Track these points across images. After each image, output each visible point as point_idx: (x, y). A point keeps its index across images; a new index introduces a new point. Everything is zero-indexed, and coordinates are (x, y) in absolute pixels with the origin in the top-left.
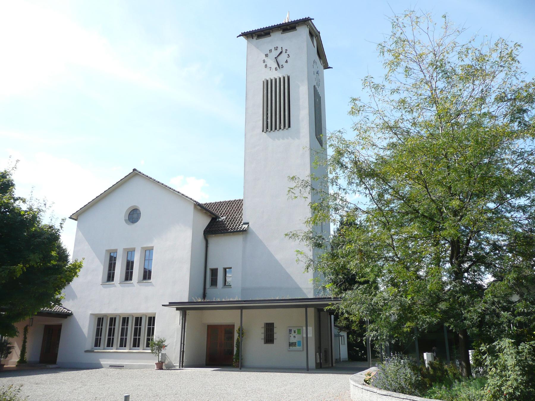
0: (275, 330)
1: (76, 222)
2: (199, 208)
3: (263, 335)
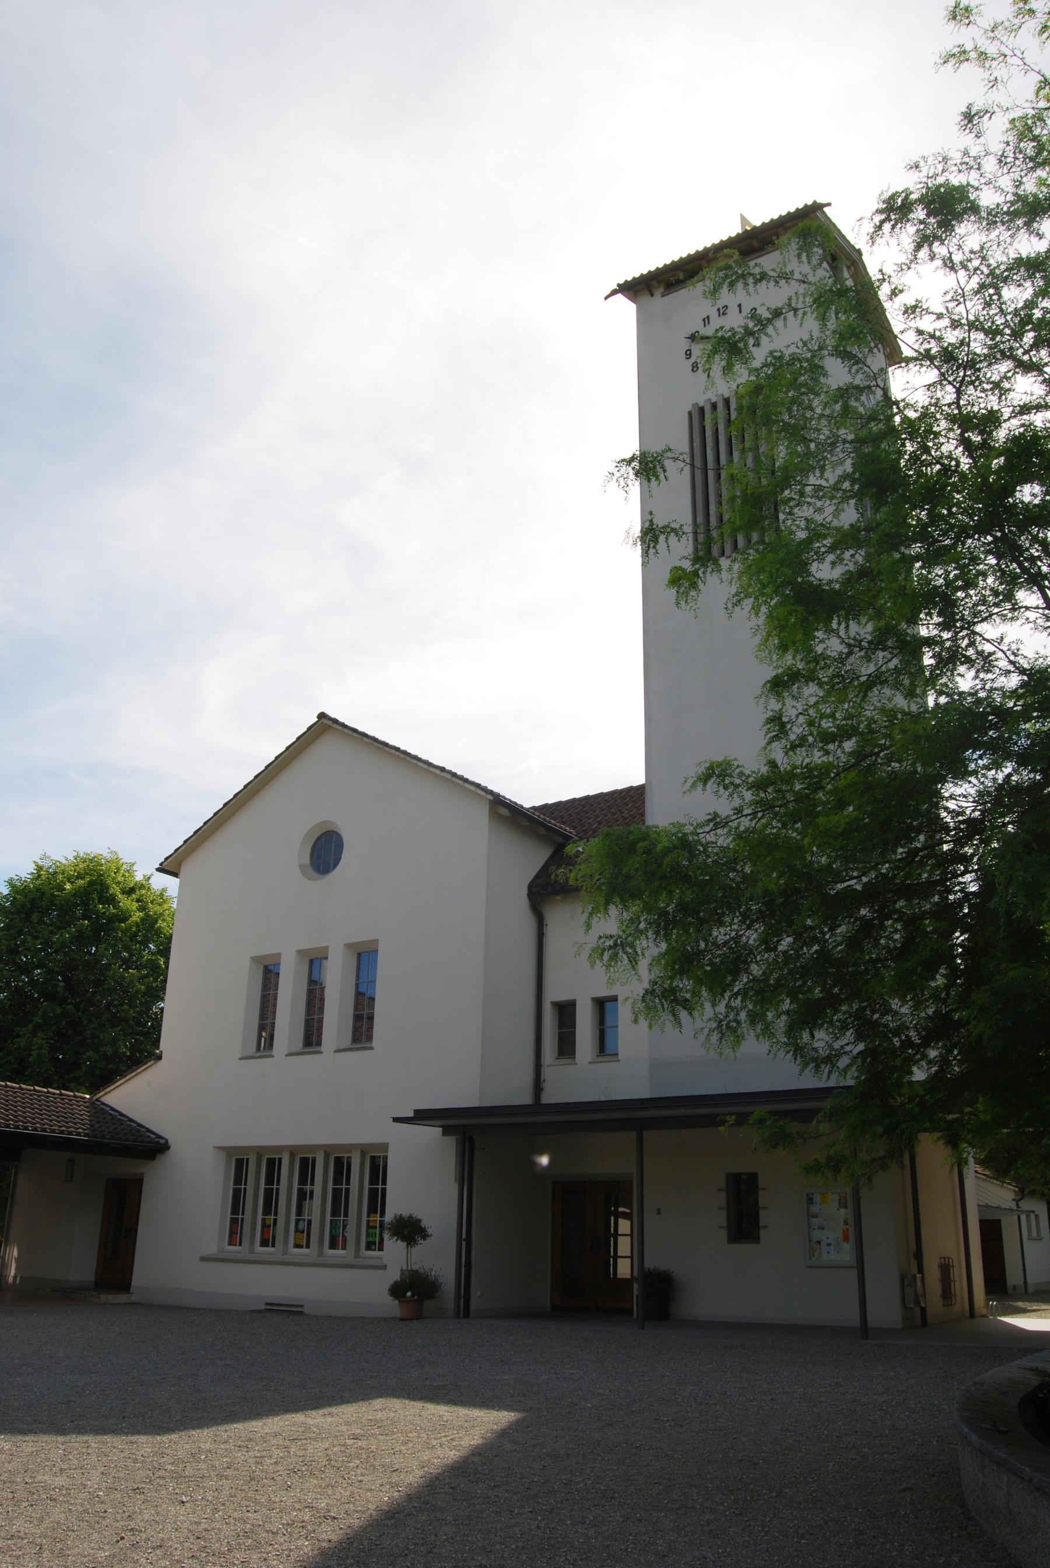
0: (763, 1198)
1: (177, 880)
2: (504, 812)
3: (724, 1213)
